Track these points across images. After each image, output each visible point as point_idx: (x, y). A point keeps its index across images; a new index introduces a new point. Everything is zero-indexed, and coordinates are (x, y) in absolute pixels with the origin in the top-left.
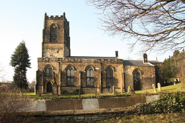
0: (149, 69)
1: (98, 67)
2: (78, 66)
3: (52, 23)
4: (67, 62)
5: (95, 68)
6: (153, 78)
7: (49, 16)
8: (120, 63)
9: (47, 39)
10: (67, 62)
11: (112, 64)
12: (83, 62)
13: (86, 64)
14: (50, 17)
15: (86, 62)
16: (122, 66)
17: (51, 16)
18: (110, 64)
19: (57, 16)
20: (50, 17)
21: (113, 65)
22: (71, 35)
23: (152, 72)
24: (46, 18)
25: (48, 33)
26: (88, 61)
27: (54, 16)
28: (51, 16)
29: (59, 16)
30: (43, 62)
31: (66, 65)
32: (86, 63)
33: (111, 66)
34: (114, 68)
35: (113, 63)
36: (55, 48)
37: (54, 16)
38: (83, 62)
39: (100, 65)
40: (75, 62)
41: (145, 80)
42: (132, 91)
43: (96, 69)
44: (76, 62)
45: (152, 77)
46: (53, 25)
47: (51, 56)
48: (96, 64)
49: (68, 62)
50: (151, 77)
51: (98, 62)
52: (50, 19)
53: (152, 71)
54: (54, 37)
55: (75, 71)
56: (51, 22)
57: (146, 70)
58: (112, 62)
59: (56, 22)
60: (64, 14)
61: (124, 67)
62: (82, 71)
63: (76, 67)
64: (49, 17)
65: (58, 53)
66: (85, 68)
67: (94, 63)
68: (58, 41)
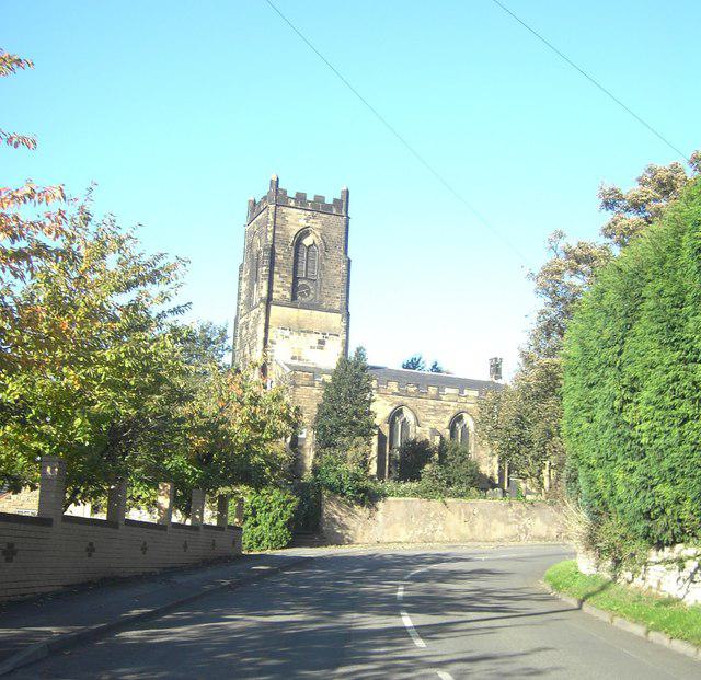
3: (303, 223)
4: (394, 394)
10: (394, 394)
12: (444, 398)
14: (331, 202)
17: (316, 197)
19: (319, 199)
22: (351, 284)
27: (310, 198)
28: (316, 197)
30: (313, 385)
31: (391, 405)
32: (453, 404)
38: (444, 398)
42: (97, 403)
46: (304, 233)
47: (294, 358)
49: (398, 395)
52: (292, 203)
59: (316, 224)
60: (347, 193)
64: (308, 199)
65: (322, 349)
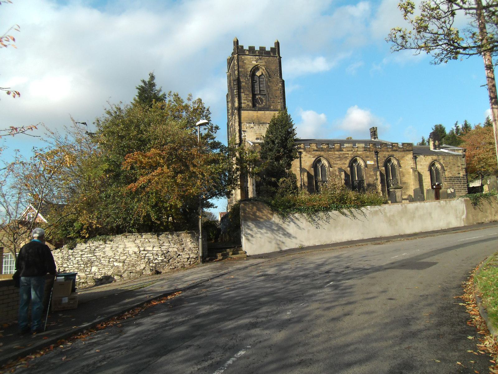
0: (455, 160)
1: (372, 159)
2: (337, 158)
3: (254, 63)
5: (365, 162)
6: (462, 177)
7: (246, 48)
8: (407, 151)
9: (246, 101)
10: (314, 150)
11: (394, 153)
12: (344, 150)
13: (350, 155)
14: (258, 49)
15: (350, 149)
16: (410, 156)
17: (260, 48)
18: (391, 153)
19: (262, 49)
20: (258, 49)
21: (397, 154)
23: (459, 166)
24: (239, 50)
25: (246, 86)
26: (353, 148)
27: (257, 49)
28: (260, 48)
29: (268, 49)
31: (314, 157)
33: (392, 156)
34: (398, 161)
35: (396, 151)
36: (265, 121)
37: (257, 49)
38: (344, 150)
39: (373, 154)
40: (329, 149)
41: (450, 181)
43: (369, 163)
44: (332, 150)
45: (461, 175)
46: (256, 68)
48: (368, 153)
49: (317, 151)
50: (458, 175)
51: (371, 150)
52: (247, 53)
53: (459, 165)
54: (260, 96)
55: (331, 169)
56: (251, 62)
57: (450, 163)
58: (394, 148)
61: (415, 158)
62: (412, 167)
63: (332, 161)
64: (256, 49)
66: (348, 162)
67: (365, 150)
68: (270, 106)
